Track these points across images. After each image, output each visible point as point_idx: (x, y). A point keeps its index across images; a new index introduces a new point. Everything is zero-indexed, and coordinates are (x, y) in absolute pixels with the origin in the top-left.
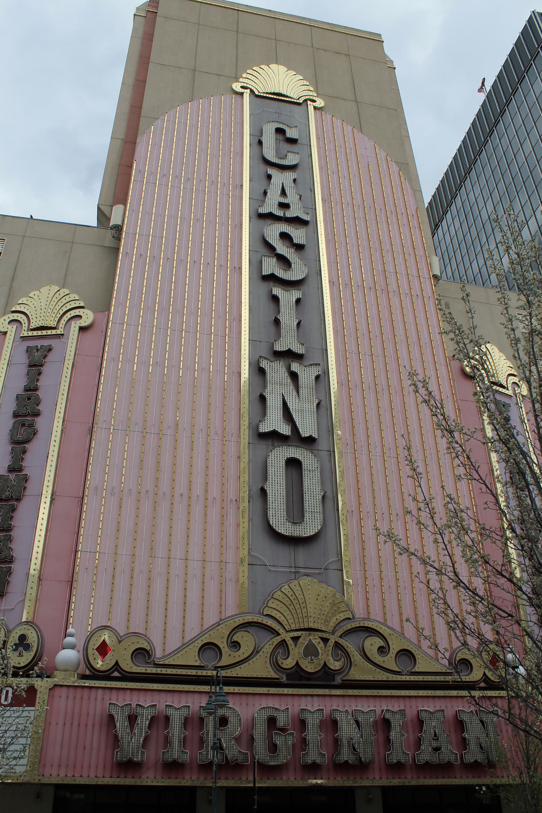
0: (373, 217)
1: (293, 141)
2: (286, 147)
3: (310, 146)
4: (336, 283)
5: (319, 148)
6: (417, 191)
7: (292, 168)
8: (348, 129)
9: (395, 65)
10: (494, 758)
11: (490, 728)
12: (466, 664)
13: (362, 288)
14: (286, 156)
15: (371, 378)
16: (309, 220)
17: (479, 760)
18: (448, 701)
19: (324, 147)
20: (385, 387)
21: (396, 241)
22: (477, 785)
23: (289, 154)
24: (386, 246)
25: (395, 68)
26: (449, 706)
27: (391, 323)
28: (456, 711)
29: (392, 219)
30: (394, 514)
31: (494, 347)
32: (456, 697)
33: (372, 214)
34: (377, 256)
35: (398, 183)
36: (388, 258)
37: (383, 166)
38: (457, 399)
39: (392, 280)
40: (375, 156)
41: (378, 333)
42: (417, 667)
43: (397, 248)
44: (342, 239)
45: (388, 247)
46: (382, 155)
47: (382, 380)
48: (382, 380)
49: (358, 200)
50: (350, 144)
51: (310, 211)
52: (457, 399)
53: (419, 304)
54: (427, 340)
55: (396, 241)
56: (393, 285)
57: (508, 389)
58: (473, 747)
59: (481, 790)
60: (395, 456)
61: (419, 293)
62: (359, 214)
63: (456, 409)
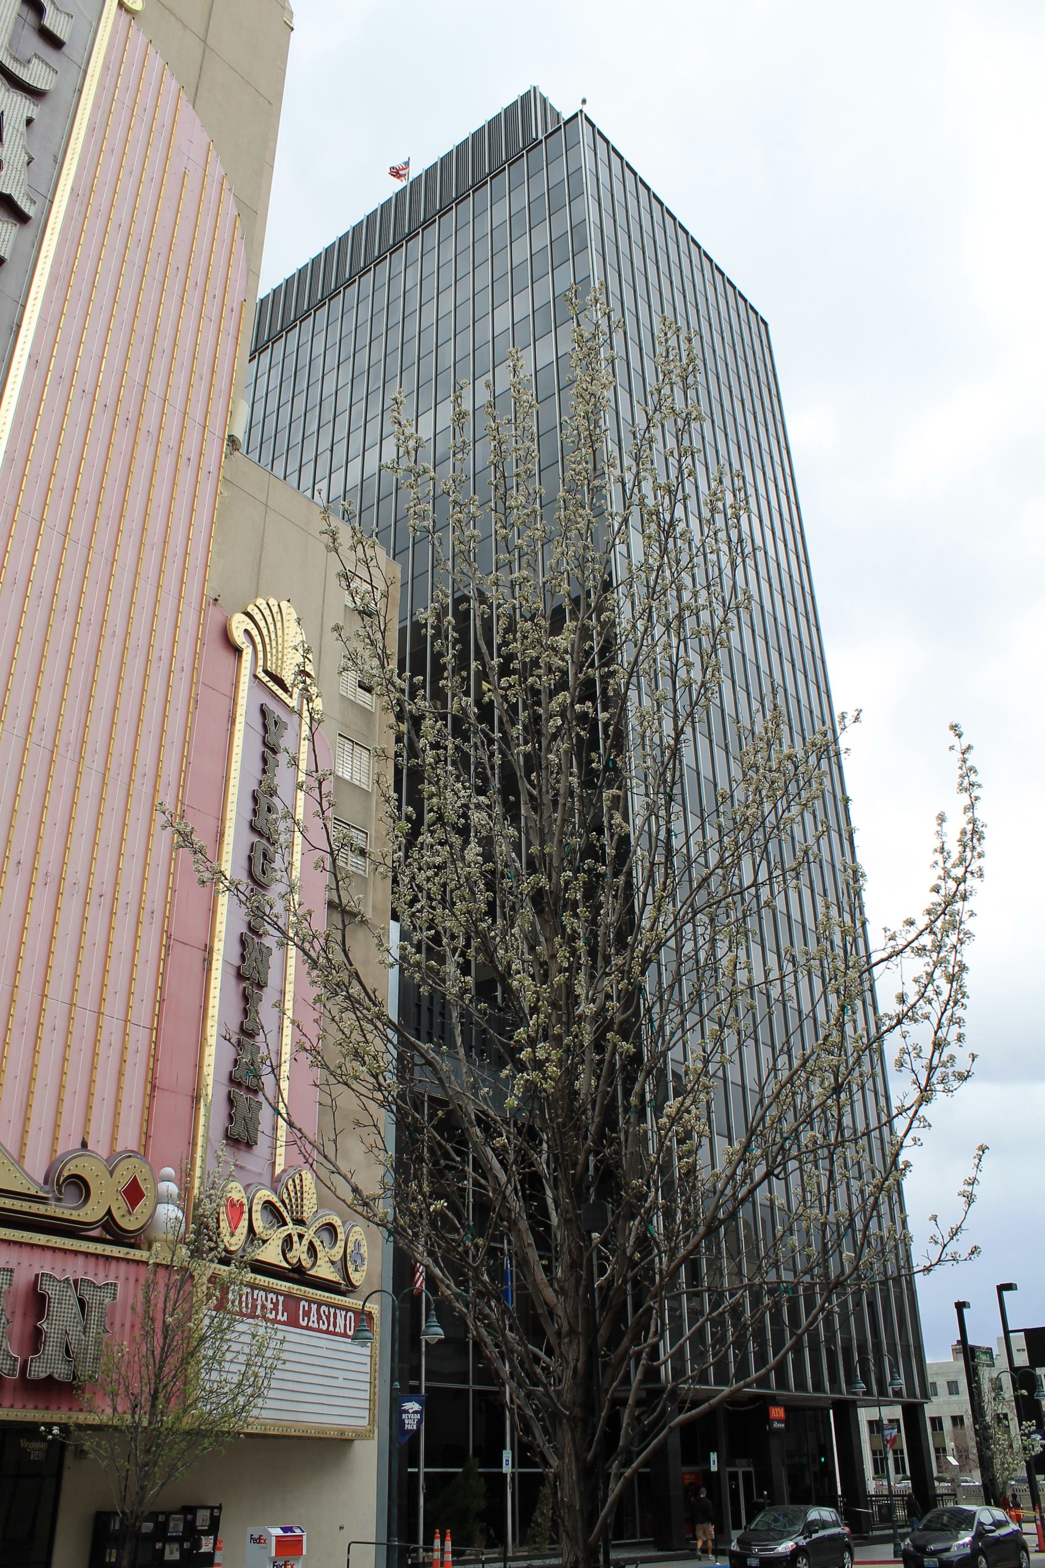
0: (158, 275)
1: (54, 42)
2: (34, 44)
3: (85, 72)
4: (42, 364)
5: (101, 87)
6: (253, 273)
7: (35, 94)
8: (172, 85)
9: (296, 23)
10: (85, 1371)
11: (94, 1317)
12: (80, 1185)
13: (90, 397)
14: (29, 62)
15: (48, 579)
16: (31, 214)
17: (56, 1376)
18: (26, 1252)
19: (112, 91)
20: (71, 605)
21: (186, 343)
22: (44, 1424)
23: (35, 61)
24: (164, 342)
25: (292, 29)
26: (25, 1263)
27: (123, 489)
28: (37, 1276)
29: (193, 298)
30: (148, 910)
31: (292, 610)
32: (43, 1248)
33: (159, 269)
34: (139, 351)
35: (227, 237)
36: (160, 366)
37: (212, 192)
38: (198, 680)
39: (153, 409)
40: (202, 163)
41: (92, 498)
42: (315, 1268)
43: (183, 356)
44: (85, 287)
45: (167, 344)
46: (216, 170)
47: (68, 591)
48: (68, 591)
49: (141, 228)
50: (164, 115)
51: (39, 200)
52: (198, 680)
53: (187, 475)
54: (180, 550)
55: (186, 343)
56: (150, 420)
57: (291, 696)
58: (52, 1348)
59: (50, 1432)
60: (49, 746)
61: (194, 456)
62: (136, 256)
63: (190, 697)
